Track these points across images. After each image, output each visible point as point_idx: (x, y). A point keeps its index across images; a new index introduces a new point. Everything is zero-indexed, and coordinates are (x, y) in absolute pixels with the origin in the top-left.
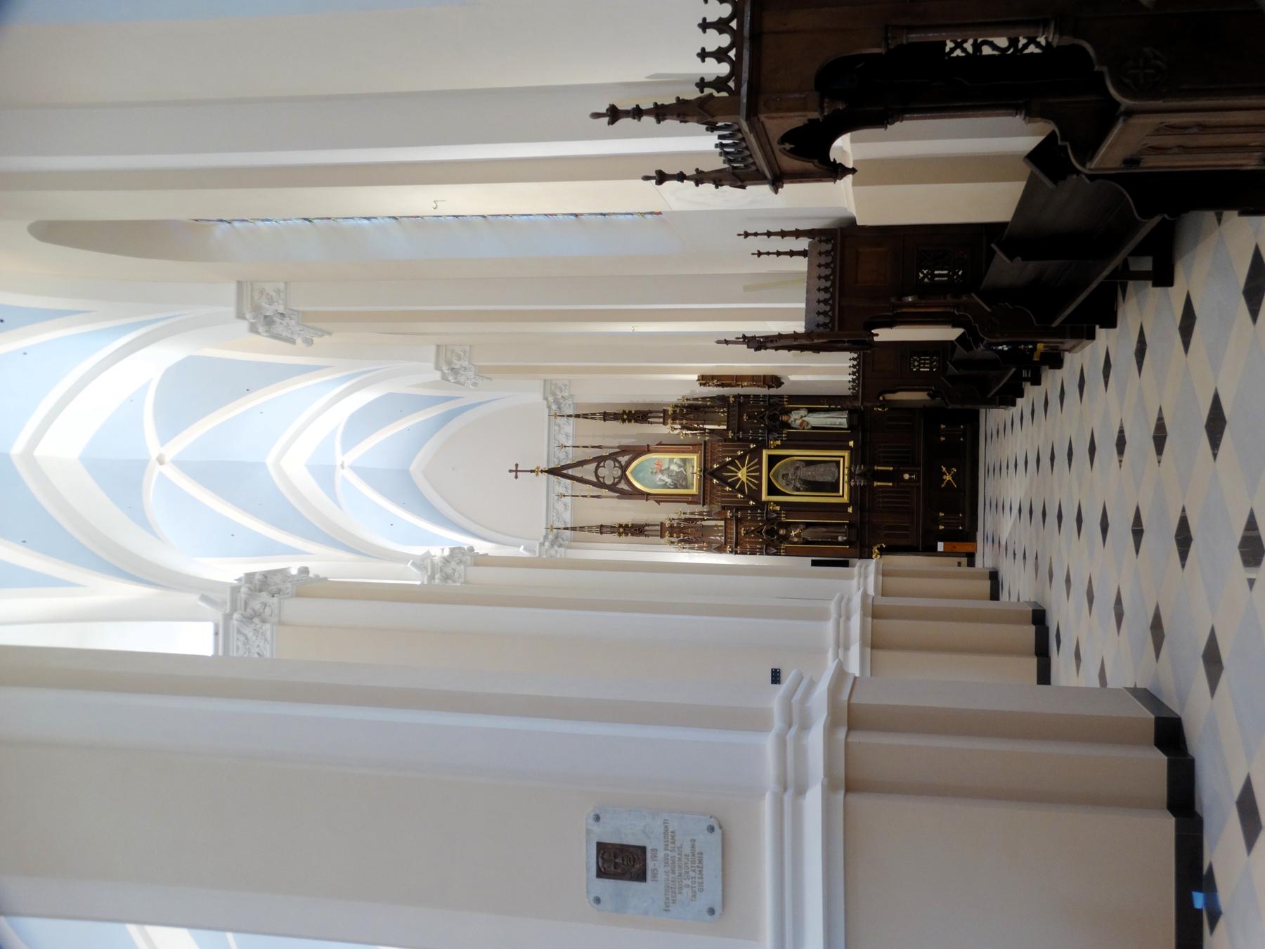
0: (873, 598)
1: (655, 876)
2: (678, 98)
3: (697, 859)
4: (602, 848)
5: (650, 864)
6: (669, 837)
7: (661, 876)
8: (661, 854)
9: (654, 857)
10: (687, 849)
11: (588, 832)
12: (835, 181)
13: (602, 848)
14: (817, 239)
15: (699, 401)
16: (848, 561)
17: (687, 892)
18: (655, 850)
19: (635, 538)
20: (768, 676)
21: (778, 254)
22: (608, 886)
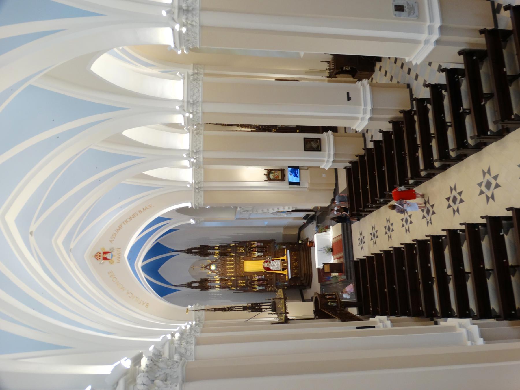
0: (319, 168)
1: (406, 11)
2: (436, 323)
3: (413, 8)
4: (396, 6)
5: (405, 9)
6: (408, 4)
7: (407, 10)
8: (407, 7)
9: (406, 8)
10: (411, 6)
11: (392, 3)
12: (111, 371)
13: (396, 6)
14: (286, 297)
15: (229, 264)
16: (318, 140)
17: (412, 13)
18: (406, 6)
19: (270, 181)
20: (400, 3)
21: (216, 310)
22: (397, 13)
